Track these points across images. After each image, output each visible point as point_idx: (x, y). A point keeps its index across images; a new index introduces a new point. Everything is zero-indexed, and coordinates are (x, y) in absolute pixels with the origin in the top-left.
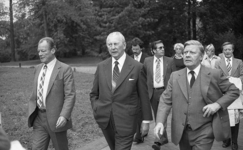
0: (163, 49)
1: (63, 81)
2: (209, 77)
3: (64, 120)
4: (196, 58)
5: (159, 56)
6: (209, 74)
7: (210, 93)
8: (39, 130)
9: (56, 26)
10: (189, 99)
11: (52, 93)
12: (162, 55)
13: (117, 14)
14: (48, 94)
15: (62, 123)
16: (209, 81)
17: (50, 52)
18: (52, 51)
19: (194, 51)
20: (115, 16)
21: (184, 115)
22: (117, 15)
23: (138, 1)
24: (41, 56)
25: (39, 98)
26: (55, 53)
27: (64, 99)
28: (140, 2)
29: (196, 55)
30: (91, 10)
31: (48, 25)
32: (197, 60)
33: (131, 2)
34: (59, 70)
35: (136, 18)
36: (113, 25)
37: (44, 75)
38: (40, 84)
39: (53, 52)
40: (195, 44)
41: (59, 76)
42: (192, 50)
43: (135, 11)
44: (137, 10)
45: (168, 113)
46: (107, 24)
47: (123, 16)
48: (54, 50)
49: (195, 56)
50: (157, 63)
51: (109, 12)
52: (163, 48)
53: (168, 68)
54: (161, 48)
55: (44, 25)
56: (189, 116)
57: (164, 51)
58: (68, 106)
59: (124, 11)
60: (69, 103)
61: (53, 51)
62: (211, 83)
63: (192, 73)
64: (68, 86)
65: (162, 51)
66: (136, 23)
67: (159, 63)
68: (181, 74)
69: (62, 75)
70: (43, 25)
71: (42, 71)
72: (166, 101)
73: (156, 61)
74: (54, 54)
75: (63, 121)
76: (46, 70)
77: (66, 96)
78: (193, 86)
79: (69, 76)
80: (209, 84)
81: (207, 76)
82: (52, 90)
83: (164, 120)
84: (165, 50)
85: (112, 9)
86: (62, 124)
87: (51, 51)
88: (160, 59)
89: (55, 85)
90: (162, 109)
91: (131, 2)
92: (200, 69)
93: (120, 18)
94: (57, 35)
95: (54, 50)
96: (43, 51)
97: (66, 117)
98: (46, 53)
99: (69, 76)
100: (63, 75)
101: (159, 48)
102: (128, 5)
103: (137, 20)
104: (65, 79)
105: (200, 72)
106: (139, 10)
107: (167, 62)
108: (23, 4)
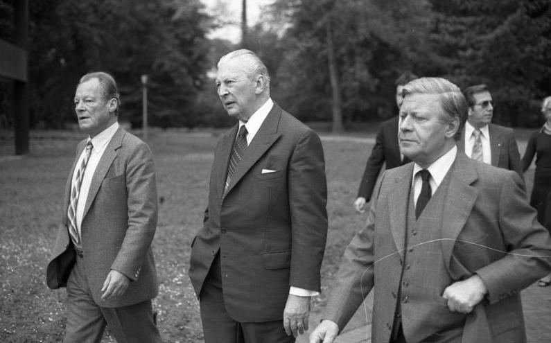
0: (490, 107)
1: (125, 178)
2: (469, 192)
3: (120, 280)
4: (429, 134)
5: (478, 125)
6: (472, 184)
7: (469, 240)
8: (76, 299)
9: (351, 54)
10: (408, 252)
11: (98, 211)
12: (487, 121)
13: (489, 30)
14: (88, 208)
15: (115, 287)
16: (470, 203)
17: (104, 106)
18: (109, 105)
19: (421, 111)
20: (482, 33)
21: (392, 297)
22: (492, 32)
23: (536, 3)
24: (81, 111)
25: (70, 222)
26: (120, 107)
27: (127, 227)
28: (541, 4)
29: (428, 124)
30: (428, 20)
31: (335, 51)
32: (433, 136)
33: (521, 3)
34: (115, 154)
35: (531, 38)
36: (480, 53)
37: (84, 166)
38: (74, 188)
39: (112, 105)
40: (429, 91)
41: (116, 167)
42: (416, 108)
43: (529, 24)
44: (533, 22)
45: (362, 290)
46: (469, 52)
47: (505, 35)
48: (114, 102)
49: (425, 128)
50: (473, 140)
51: (472, 26)
52: (490, 104)
53: (501, 153)
54: (485, 104)
55: (329, 51)
56: (406, 302)
57: (491, 113)
58: (132, 243)
59: (506, 23)
60: (135, 237)
61: (112, 104)
62: (475, 210)
63: (426, 176)
64: (139, 194)
65: (487, 113)
66: (532, 52)
67: (479, 141)
68: (400, 178)
69: (122, 166)
70: (325, 52)
71: (84, 155)
72: (360, 257)
73: (473, 134)
74: (116, 111)
75: (116, 283)
76: (90, 153)
77: (130, 219)
78: (422, 216)
79: (137, 169)
80: (467, 213)
81: (467, 191)
82: (98, 202)
83: (340, 312)
84: (495, 111)
85: (479, 19)
86: (115, 291)
87: (107, 103)
88: (482, 130)
89: (102, 189)
90: (341, 281)
91: (521, 3)
92: (453, 166)
93: (497, 38)
94: (354, 74)
95: (114, 102)
96: (90, 101)
97: (127, 274)
98: (95, 104)
99: (137, 169)
100: (126, 166)
101: (479, 104)
102: (514, 11)
103: (534, 43)
104: (129, 175)
105: (450, 175)
106: (538, 21)
107: (499, 138)
108: (278, 7)
